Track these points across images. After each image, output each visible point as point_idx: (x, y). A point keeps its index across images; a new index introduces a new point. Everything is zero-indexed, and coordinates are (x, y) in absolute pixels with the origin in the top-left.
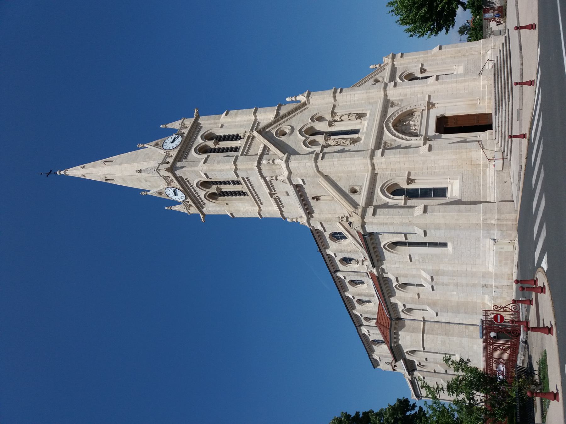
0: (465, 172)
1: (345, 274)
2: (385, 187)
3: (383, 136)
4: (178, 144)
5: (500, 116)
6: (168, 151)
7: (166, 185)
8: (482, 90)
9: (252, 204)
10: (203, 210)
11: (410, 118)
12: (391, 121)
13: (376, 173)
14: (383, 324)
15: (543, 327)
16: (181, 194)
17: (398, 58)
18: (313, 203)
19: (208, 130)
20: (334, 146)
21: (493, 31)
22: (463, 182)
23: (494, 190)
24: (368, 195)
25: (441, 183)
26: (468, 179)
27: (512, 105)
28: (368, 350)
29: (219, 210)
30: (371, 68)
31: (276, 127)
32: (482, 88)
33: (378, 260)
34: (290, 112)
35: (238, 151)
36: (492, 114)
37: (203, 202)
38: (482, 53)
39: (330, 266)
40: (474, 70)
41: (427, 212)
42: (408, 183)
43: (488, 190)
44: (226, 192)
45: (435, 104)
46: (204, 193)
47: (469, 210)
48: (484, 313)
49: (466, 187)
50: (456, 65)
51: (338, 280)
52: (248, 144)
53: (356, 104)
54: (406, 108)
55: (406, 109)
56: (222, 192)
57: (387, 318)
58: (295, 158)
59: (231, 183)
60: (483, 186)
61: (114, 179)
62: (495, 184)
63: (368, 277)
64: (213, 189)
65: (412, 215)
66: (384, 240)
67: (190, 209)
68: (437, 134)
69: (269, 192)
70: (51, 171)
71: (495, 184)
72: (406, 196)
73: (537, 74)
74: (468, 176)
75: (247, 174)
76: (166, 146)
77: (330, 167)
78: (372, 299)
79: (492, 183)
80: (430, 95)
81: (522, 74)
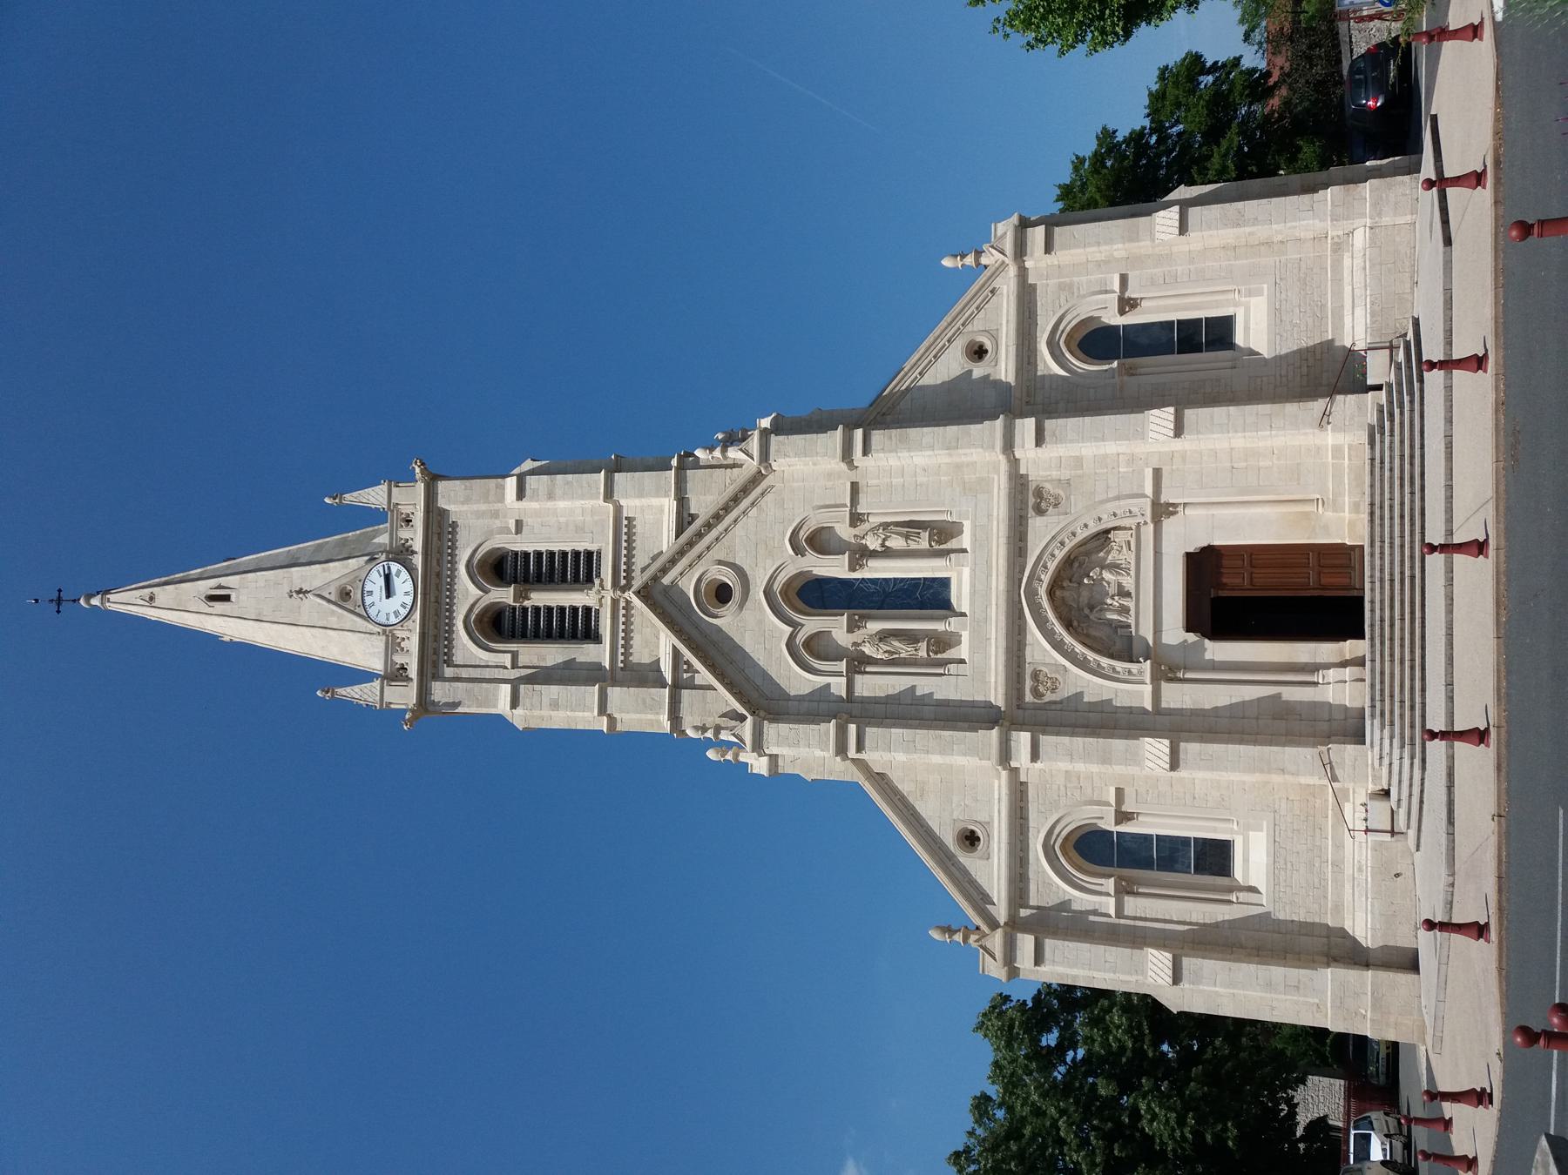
0: (1283, 806)
2: (1059, 332)
3: (1025, 645)
5: (1384, 754)
6: (388, 628)
8: (1333, 464)
11: (1102, 554)
12: (1043, 577)
13: (1021, 473)
17: (1036, 254)
19: (478, 542)
22: (1277, 844)
23: (1364, 899)
24: (1011, 868)
25: (1218, 304)
30: (943, 266)
32: (1332, 459)
36: (1362, 547)
38: (1333, 238)
41: (1178, 767)
42: (1122, 312)
43: (1348, 887)
45: (1178, 509)
47: (1295, 986)
49: (1286, 864)
50: (1243, 288)
52: (622, 627)
53: (921, 485)
54: (1084, 522)
55: (1086, 526)
60: (1335, 869)
62: (1369, 879)
65: (1142, 974)
68: (1192, 637)
71: (1369, 879)
74: (1292, 823)
79: (1360, 870)
80: (1158, 469)
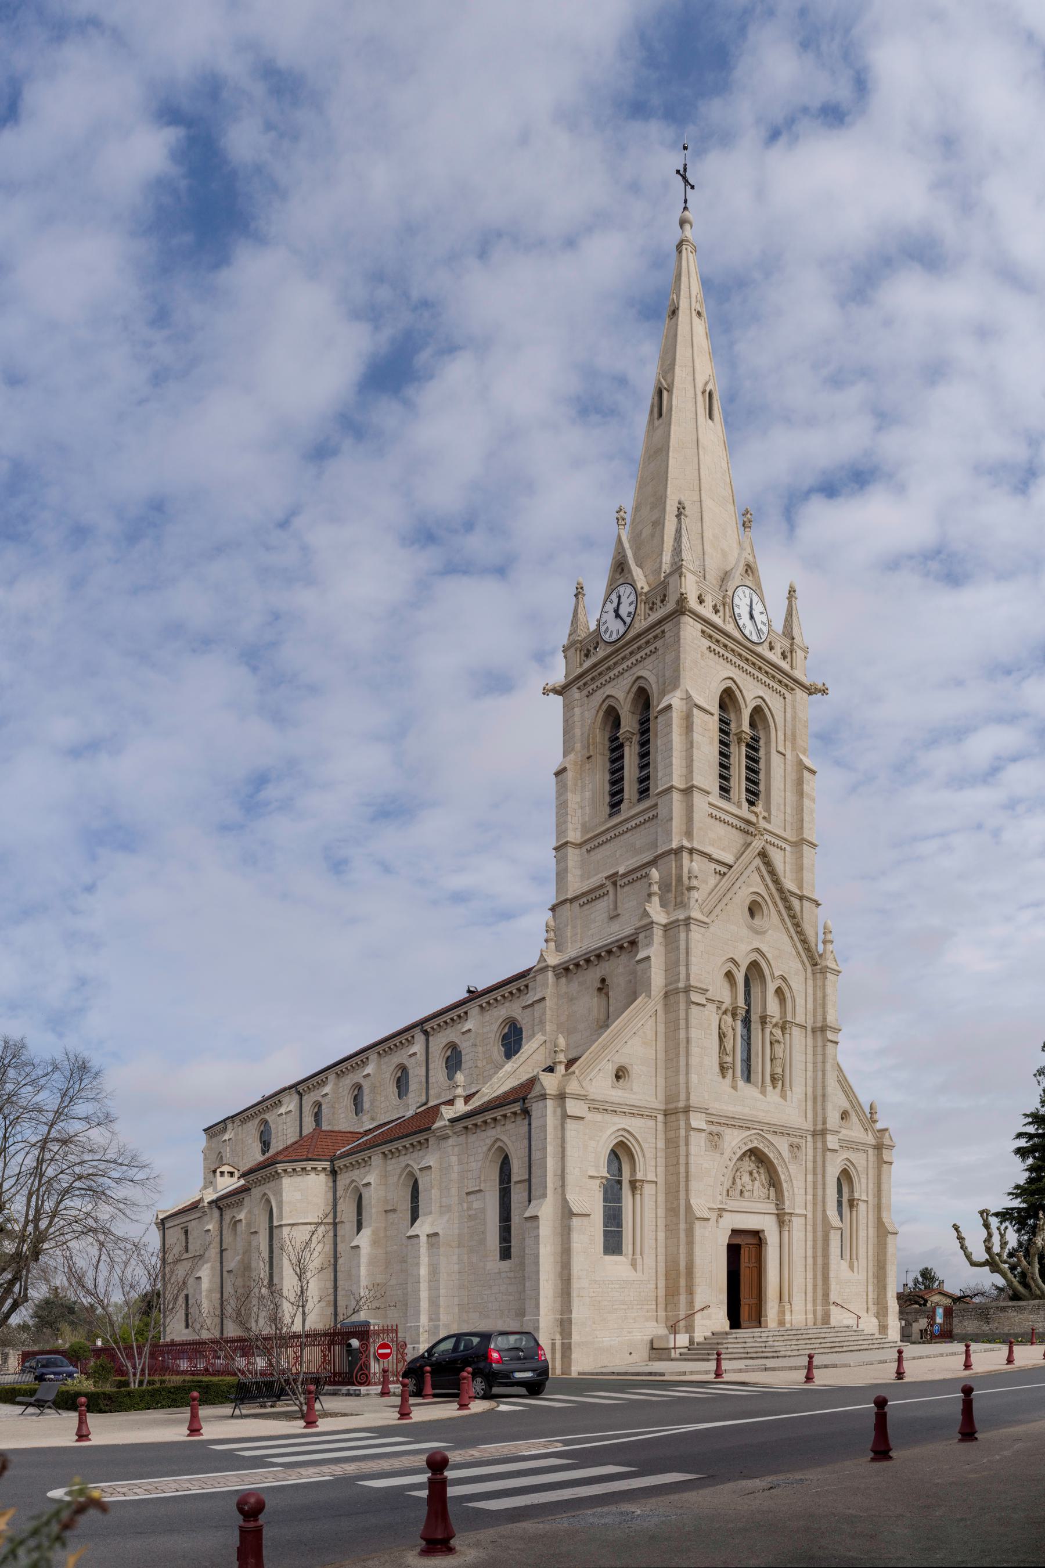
1: (421, 1057)
4: (747, 633)
7: (642, 588)
9: (588, 825)
10: (574, 688)
14: (319, 1140)
15: (400, 1398)
16: (618, 631)
18: (592, 976)
20: (720, 1029)
21: (911, 1325)
26: (638, 1290)
27: (773, 1357)
28: (245, 1115)
29: (574, 733)
31: (771, 895)
33: (466, 1128)
34: (799, 929)
35: (721, 796)
37: (594, 691)
39: (440, 1020)
40: (844, 1294)
44: (622, 757)
46: (620, 695)
48: (388, 1326)
51: (407, 1039)
56: (622, 746)
57: (333, 1151)
58: (698, 941)
59: (642, 774)
61: (661, 420)
63: (418, 1104)
64: (629, 723)
66: (416, 1161)
67: (578, 652)
69: (620, 873)
70: (693, 187)
72: (607, 1179)
73: (825, 1386)
75: (665, 820)
76: (742, 596)
77: (674, 1021)
78: (365, 1118)
81: (826, 1367)
